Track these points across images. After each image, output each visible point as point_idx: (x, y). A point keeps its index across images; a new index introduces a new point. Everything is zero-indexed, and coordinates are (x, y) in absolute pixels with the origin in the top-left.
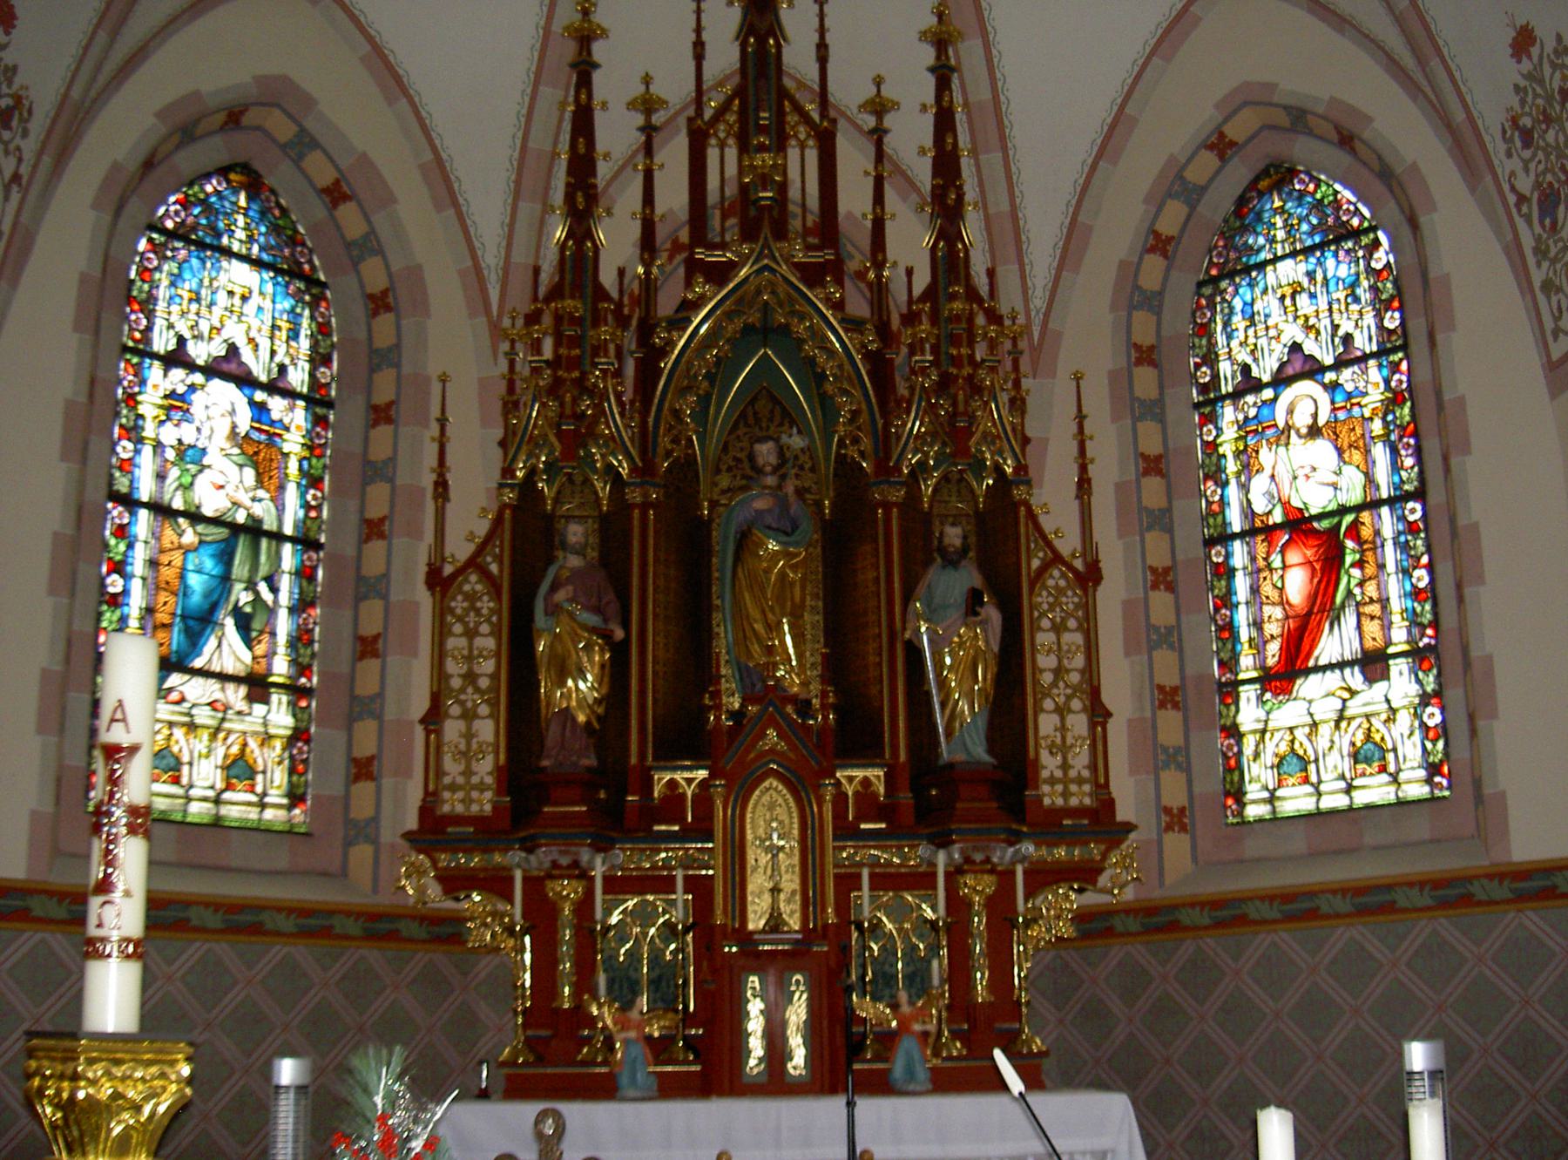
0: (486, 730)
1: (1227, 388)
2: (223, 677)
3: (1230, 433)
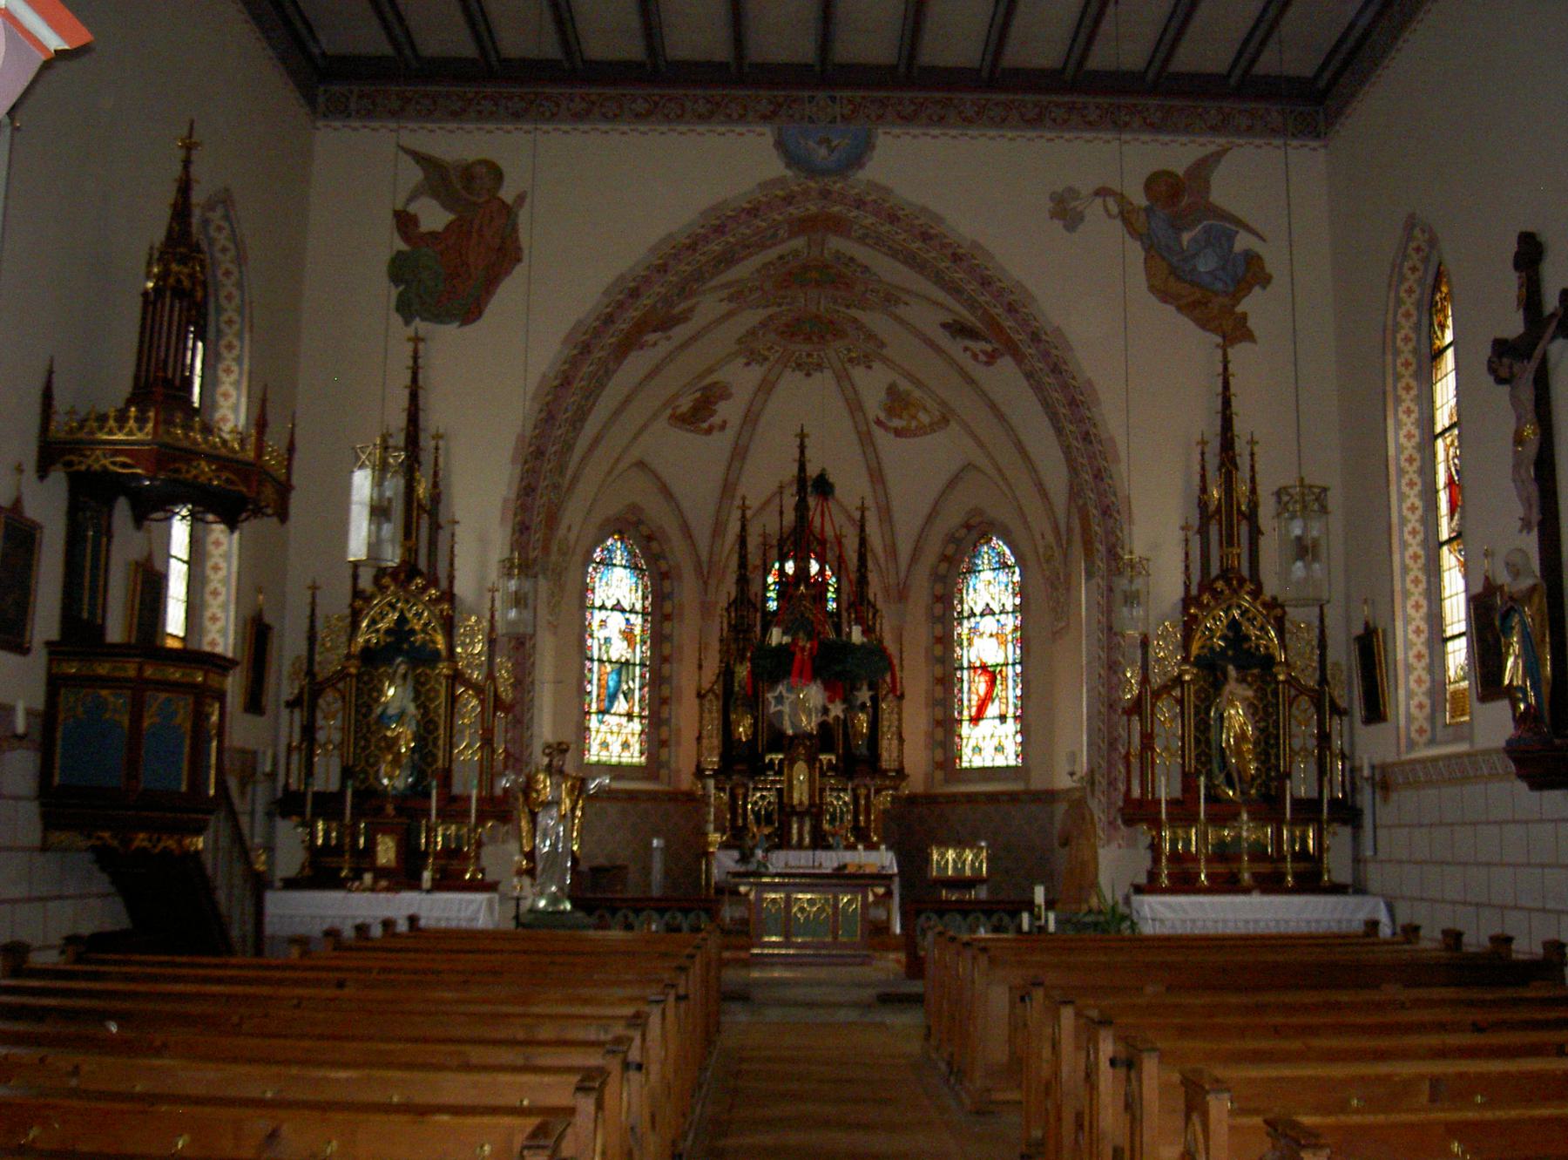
3: (966, 631)
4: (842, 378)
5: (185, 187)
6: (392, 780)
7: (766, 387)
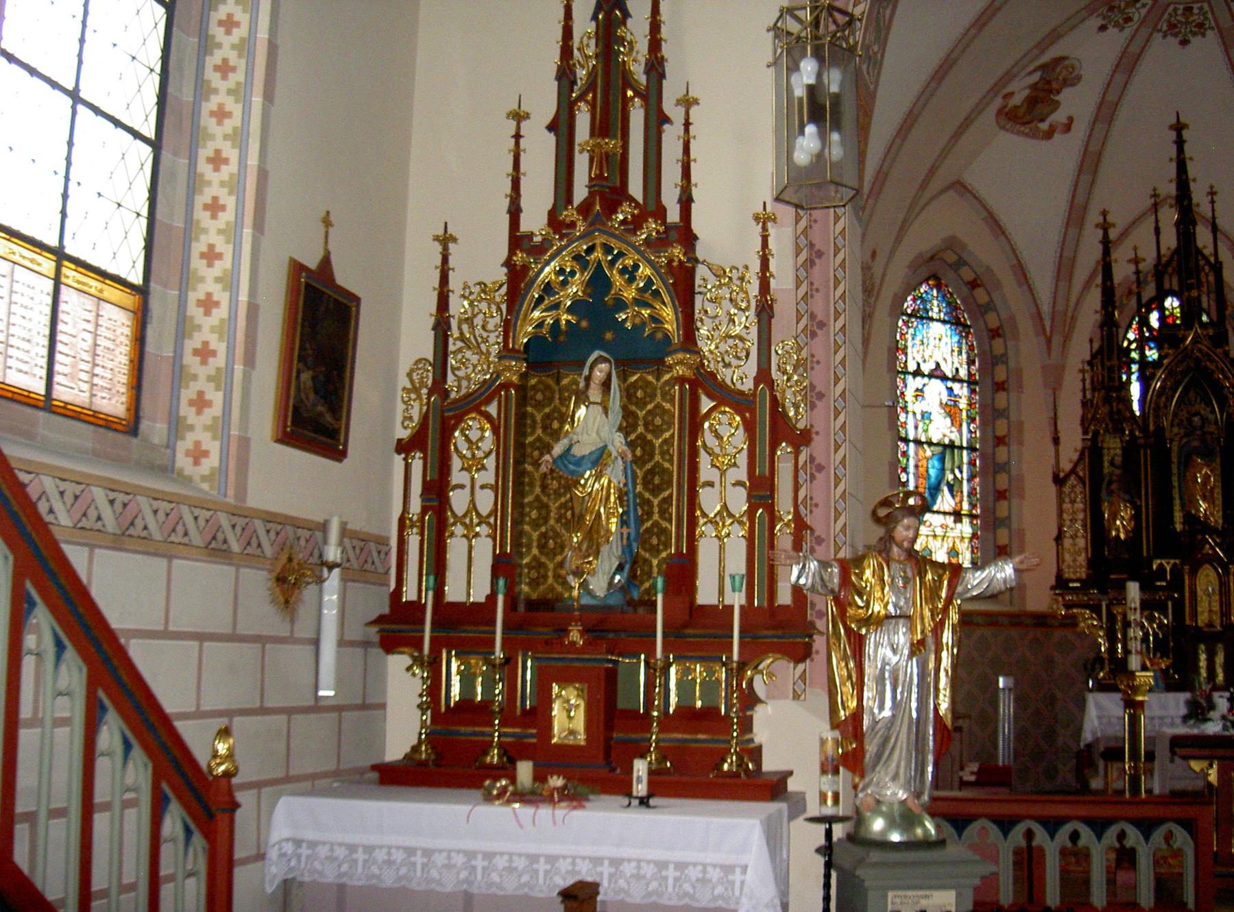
2: (945, 513)
6: (600, 579)
7: (1127, 64)
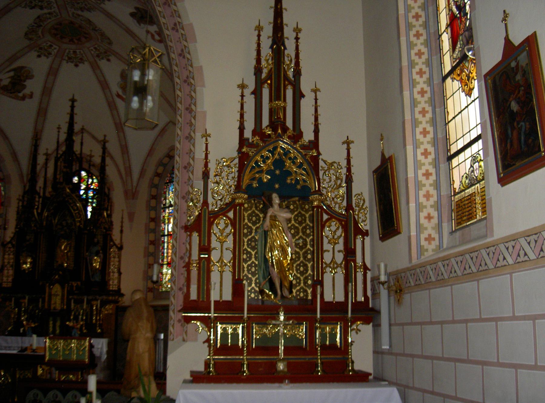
0: (11, 272)
1: (167, 205)
3: (167, 215)
4: (95, 67)
5: (58, 139)
7: (53, 72)
